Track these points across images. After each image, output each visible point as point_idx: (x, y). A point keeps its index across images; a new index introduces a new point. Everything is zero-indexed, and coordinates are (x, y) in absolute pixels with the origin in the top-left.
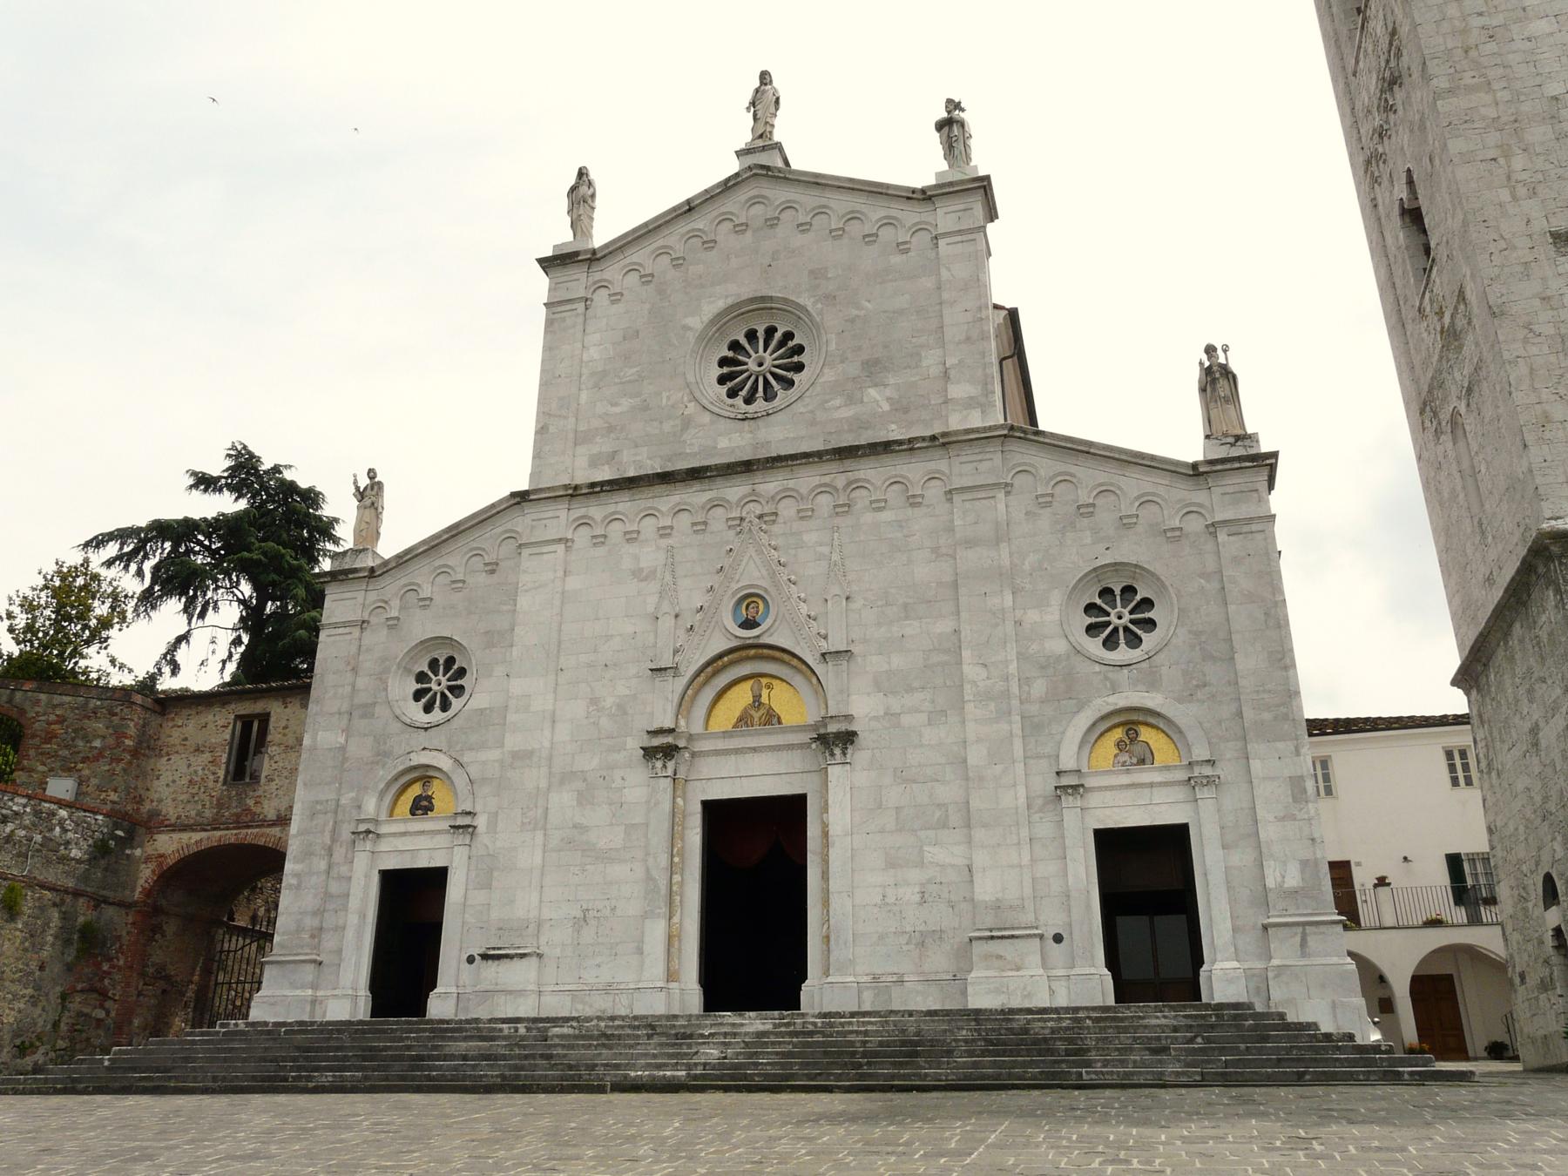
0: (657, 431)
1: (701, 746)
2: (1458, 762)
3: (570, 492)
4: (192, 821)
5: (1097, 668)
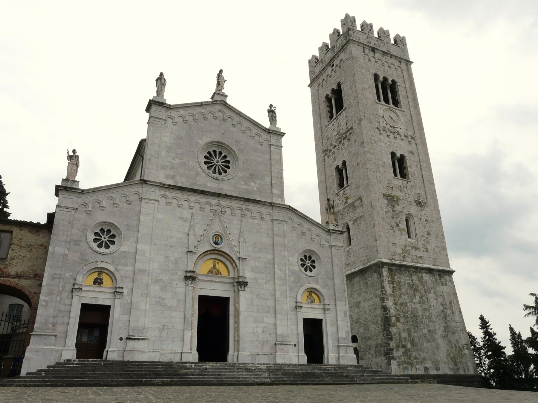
0: (188, 174)
3: (162, 185)
5: (305, 276)
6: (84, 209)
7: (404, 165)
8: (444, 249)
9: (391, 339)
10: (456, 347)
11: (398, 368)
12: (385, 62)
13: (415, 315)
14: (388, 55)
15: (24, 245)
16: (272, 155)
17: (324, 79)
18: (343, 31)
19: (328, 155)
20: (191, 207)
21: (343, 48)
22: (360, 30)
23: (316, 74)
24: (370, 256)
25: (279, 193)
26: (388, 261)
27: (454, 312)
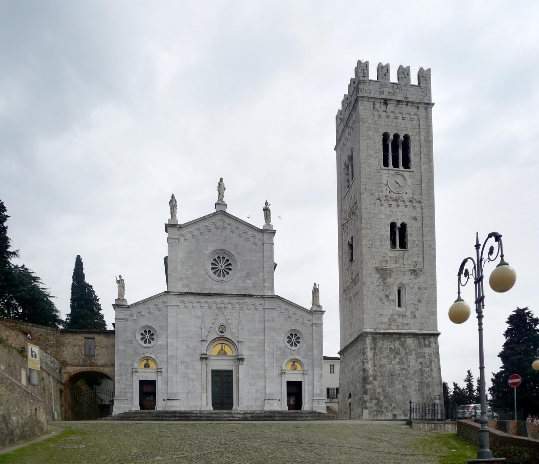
1: (212, 358)
2: (332, 368)
4: (77, 364)
5: (289, 350)
6: (132, 318)
9: (366, 393)
15: (102, 346)
16: (265, 253)
20: (202, 307)
26: (372, 330)
27: (433, 369)
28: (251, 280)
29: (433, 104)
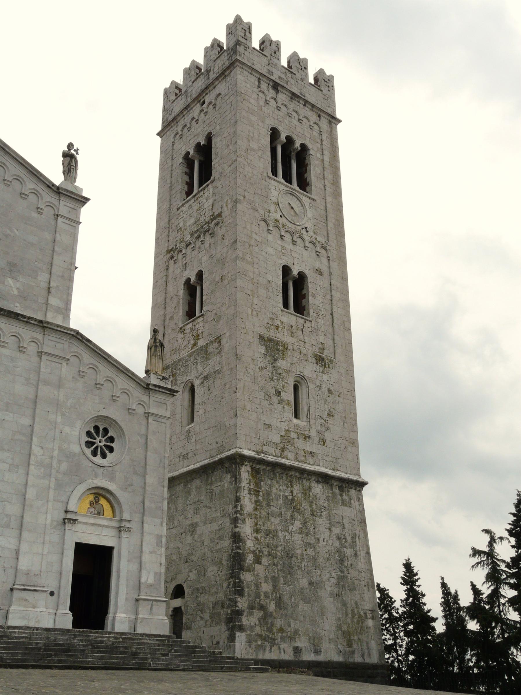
5: (91, 464)
7: (304, 292)
8: (354, 443)
9: (241, 593)
10: (353, 614)
11: (248, 647)
12: (294, 111)
13: (288, 554)
14: (301, 101)
17: (186, 126)
18: (227, 45)
19: (175, 258)
21: (223, 74)
22: (258, 48)
23: (174, 115)
24: (224, 443)
25: (61, 304)
27: (358, 553)
28: (18, 281)
29: (81, 223)
